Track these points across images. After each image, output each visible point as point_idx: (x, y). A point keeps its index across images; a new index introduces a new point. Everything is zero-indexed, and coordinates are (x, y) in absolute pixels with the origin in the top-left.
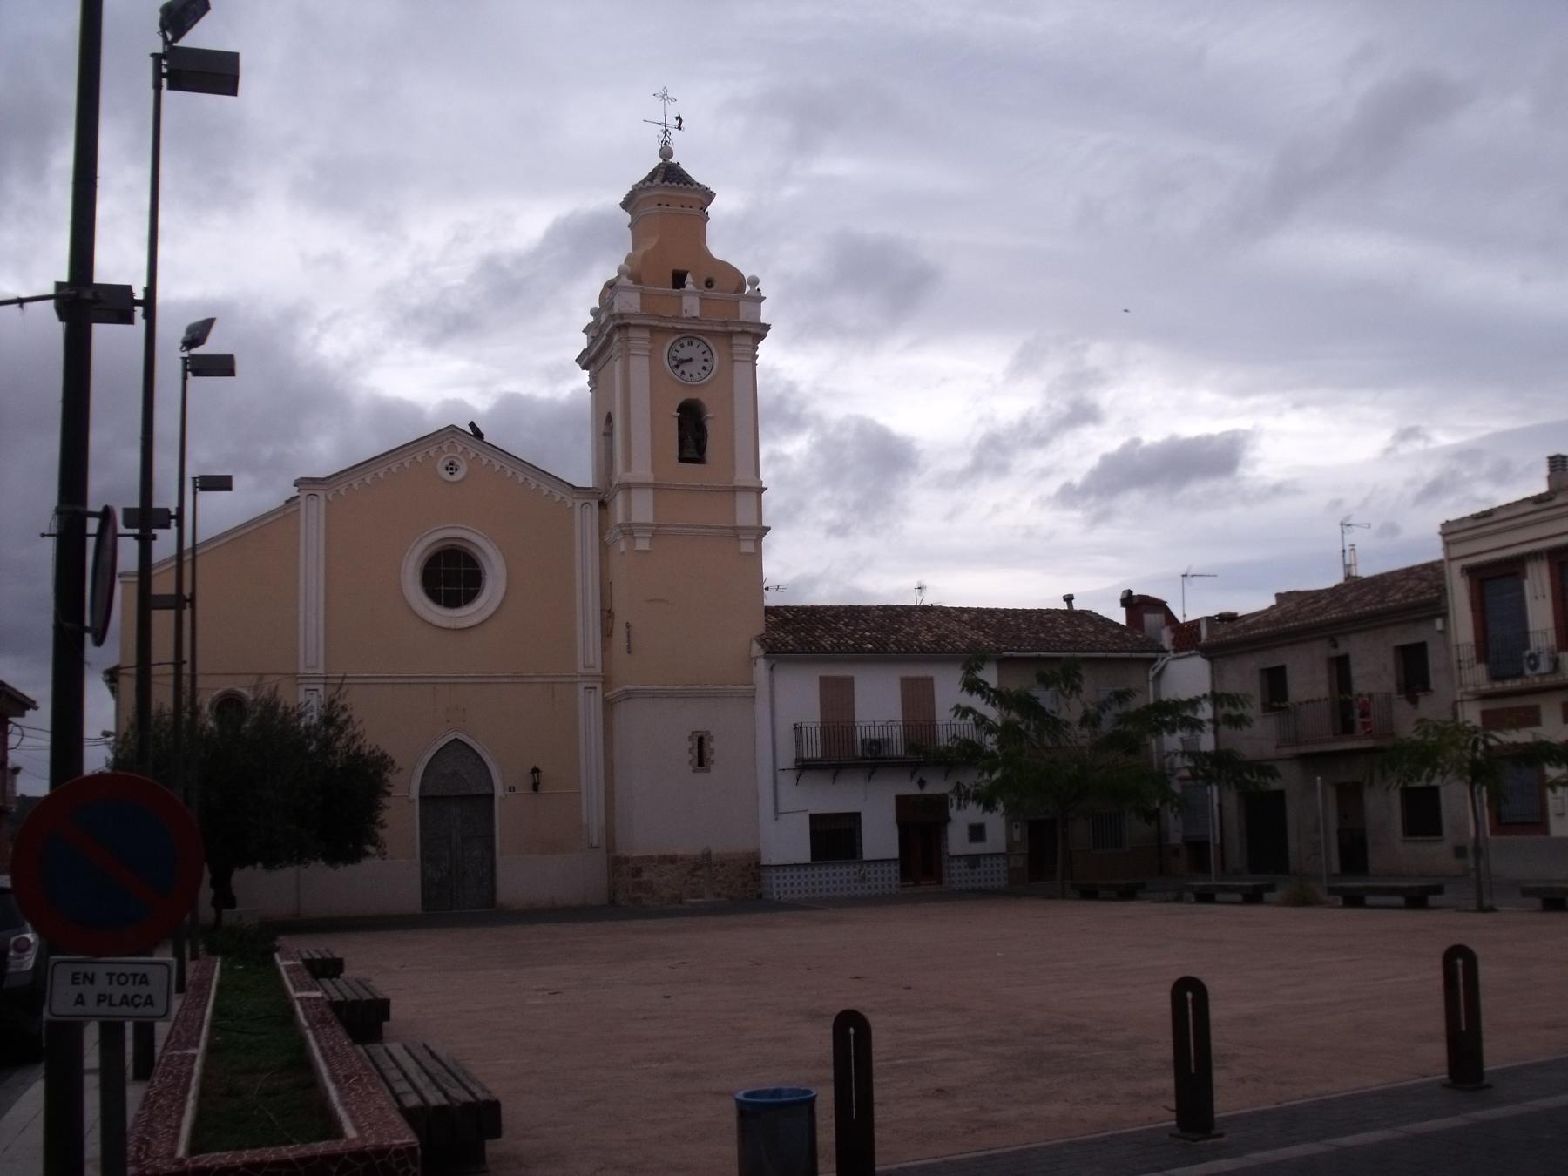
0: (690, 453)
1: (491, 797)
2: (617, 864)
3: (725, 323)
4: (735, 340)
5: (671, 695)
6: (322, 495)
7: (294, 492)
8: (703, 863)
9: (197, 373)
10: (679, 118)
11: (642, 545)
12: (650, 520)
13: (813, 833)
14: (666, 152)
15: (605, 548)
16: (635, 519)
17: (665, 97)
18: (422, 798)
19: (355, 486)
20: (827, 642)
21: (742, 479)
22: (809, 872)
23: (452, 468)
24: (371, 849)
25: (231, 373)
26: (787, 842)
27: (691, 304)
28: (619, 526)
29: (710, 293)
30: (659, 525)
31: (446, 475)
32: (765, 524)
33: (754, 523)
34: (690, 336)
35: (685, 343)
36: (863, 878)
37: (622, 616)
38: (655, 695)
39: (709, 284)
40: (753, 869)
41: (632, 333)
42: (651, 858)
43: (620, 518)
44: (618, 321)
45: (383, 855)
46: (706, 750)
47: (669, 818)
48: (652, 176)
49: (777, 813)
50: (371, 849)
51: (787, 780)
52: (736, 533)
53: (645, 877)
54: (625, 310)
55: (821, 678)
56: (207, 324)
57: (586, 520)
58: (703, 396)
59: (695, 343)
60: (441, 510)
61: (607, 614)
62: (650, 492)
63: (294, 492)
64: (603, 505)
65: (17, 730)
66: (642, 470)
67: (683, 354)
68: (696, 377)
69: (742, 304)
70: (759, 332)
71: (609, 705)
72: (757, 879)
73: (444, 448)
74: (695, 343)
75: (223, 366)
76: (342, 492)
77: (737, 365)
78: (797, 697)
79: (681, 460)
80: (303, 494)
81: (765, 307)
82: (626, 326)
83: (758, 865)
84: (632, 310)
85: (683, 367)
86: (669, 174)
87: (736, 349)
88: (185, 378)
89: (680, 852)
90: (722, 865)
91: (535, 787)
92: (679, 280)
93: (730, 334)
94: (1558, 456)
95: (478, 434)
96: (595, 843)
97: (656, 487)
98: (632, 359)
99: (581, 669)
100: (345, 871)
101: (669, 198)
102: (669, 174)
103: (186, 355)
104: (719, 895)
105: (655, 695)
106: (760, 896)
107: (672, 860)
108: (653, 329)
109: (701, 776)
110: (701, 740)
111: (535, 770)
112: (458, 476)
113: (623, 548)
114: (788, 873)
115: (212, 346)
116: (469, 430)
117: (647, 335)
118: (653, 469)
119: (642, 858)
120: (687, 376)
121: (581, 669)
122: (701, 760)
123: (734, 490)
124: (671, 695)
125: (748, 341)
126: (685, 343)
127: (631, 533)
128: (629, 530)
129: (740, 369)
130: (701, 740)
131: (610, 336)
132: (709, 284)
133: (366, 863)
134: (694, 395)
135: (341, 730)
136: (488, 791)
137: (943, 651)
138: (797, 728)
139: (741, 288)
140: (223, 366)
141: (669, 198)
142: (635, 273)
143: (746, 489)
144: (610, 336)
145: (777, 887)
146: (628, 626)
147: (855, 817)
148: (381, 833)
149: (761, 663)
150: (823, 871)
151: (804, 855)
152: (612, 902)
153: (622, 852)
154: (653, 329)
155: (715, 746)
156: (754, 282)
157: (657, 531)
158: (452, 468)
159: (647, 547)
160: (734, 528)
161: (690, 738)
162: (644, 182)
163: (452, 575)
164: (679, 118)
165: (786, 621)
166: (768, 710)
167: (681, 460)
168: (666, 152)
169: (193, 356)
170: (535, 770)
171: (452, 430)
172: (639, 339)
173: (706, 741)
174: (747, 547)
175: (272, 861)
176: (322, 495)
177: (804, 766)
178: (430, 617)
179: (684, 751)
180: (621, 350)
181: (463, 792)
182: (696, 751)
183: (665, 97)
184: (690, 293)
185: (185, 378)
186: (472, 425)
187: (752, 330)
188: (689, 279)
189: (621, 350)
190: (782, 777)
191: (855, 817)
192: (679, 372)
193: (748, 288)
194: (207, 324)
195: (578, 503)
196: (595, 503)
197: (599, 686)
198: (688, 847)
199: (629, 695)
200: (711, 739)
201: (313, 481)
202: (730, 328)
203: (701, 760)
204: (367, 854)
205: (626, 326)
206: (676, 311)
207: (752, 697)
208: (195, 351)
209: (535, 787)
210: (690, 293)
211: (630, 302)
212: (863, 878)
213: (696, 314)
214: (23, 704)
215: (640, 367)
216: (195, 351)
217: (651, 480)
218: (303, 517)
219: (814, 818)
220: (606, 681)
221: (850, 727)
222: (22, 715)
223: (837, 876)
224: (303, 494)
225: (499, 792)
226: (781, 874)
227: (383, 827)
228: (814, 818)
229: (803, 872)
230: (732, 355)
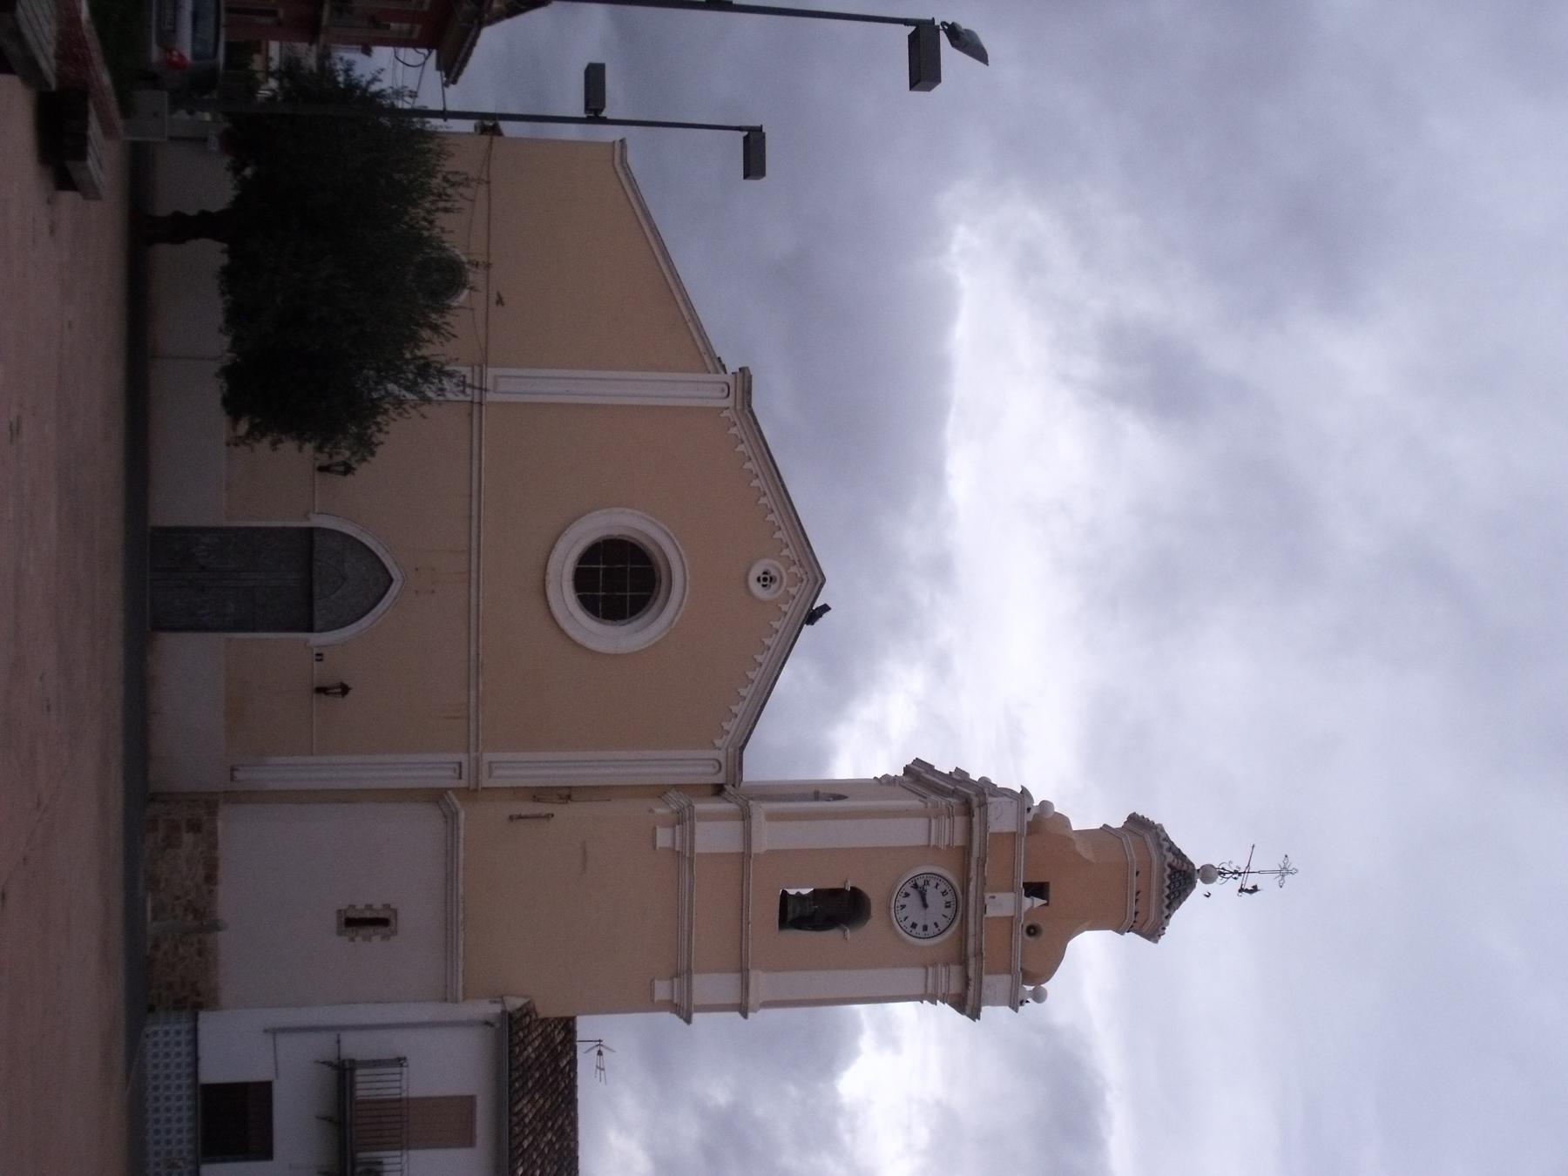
1: (310, 629)
2: (210, 803)
3: (979, 953)
4: (955, 969)
5: (450, 878)
6: (729, 402)
7: (732, 366)
8: (203, 920)
9: (913, 39)
10: (1255, 889)
11: (664, 838)
12: (698, 850)
13: (243, 1086)
14: (1209, 874)
15: (660, 792)
16: (701, 827)
17: (1284, 871)
18: (311, 530)
19: (741, 448)
20: (524, 1105)
21: (761, 981)
22: (185, 1081)
23: (766, 579)
24: (243, 426)
25: (914, 85)
26: (231, 1048)
27: (1004, 904)
28: (690, 805)
29: (1020, 935)
30: (691, 860)
31: (757, 571)
32: (696, 1017)
33: (697, 999)
34: (959, 905)
35: (949, 898)
36: (173, 1165)
37: (561, 811)
38: (450, 853)
39: (1033, 931)
41: (960, 821)
42: (214, 846)
43: (700, 807)
44: (975, 801)
45: (236, 442)
46: (371, 930)
47: (271, 876)
48: (1179, 854)
49: (274, 1032)
50: (243, 426)
51: (322, 1046)
52: (682, 973)
53: (188, 838)
54: (991, 809)
55: (470, 1100)
56: (979, 54)
57: (699, 766)
59: (949, 912)
60: (707, 564)
61: (566, 795)
62: (736, 847)
63: (732, 366)
64: (718, 790)
65: (421, 59)
66: (768, 837)
67: (933, 895)
68: (902, 915)
69: (1007, 978)
70: (967, 1004)
71: (436, 796)
72: (179, 1005)
73: (793, 569)
74: (949, 912)
75: (924, 72)
76: (733, 430)
77: (920, 972)
78: (445, 1061)
80: (729, 379)
81: (1004, 1011)
82: (969, 813)
83: (198, 1007)
84: (991, 818)
85: (914, 894)
86: (1180, 878)
87: (942, 971)
88: (906, 22)
89: (222, 891)
90: (200, 953)
91: (321, 690)
92: (1036, 889)
93: (963, 962)
95: (813, 616)
96: (239, 775)
97: (745, 856)
98: (922, 822)
99: (488, 757)
100: (212, 392)
101: (1145, 879)
102: (1180, 878)
103: (937, 23)
104: (156, 946)
105: (450, 853)
106: (151, 1009)
107: (211, 878)
108: (966, 851)
109: (332, 921)
110: (384, 922)
111: (345, 690)
112: (756, 588)
113: (659, 811)
114: (184, 1049)
115: (950, 57)
116: (818, 604)
117: (959, 841)
118: (771, 853)
119: (213, 833)
120: (902, 901)
121: (488, 757)
122: (354, 923)
123: (743, 971)
124: (450, 878)
125: (955, 987)
126: (949, 898)
127: (680, 821)
128: (683, 819)
129: (914, 977)
130: (384, 922)
131: (954, 793)
132: (1033, 931)
133: (221, 419)
134: (875, 910)
135: (411, 387)
136: (318, 623)
137: (513, 1161)
138: (400, 1061)
139: (1029, 977)
140: (924, 72)
141: (1145, 879)
142: (1041, 824)
143: (745, 987)
144: (954, 793)
145: (164, 1031)
146: (549, 816)
147: (266, 1153)
148: (266, 442)
149: (497, 1009)
150: (186, 1103)
151: (211, 1073)
152: (153, 798)
153: (224, 811)
154: (966, 851)
155: (373, 945)
156: (1039, 997)
157: (682, 857)
158: (766, 579)
159: (659, 844)
160: (689, 970)
161: (387, 907)
162: (1167, 839)
163: (619, 579)
164: (1255, 889)
165: (556, 1057)
168: (1209, 874)
169: (938, 30)
170: (345, 690)
171: (819, 581)
172: (950, 832)
173: (382, 930)
174: (662, 991)
175: (230, 277)
176: (729, 402)
177: (343, 1072)
178: (561, 546)
179: (369, 898)
180: (936, 805)
181: (317, 590)
182: (368, 915)
183: (1284, 871)
184: (1019, 905)
185: (906, 22)
186: (825, 608)
187: (971, 993)
188: (1038, 902)
189: (936, 805)
190: (326, 1040)
191: (266, 1153)
192: (908, 889)
193: (1029, 988)
194: (979, 54)
195: (720, 755)
196: (720, 779)
197: (463, 783)
198: (228, 900)
199: (451, 818)
200: (386, 937)
201: (747, 392)
202: (972, 961)
203: (354, 923)
204: (236, 420)
205: (969, 813)
206: (984, 893)
207: (447, 997)
208: (943, 38)
209: (321, 690)
210: (1019, 905)
211: (1002, 820)
212: (173, 1165)
213: (990, 913)
214: (452, 68)
215: (912, 833)
216: (943, 38)
217: (755, 850)
218: (691, 376)
219: (265, 1089)
220: (471, 793)
221: (403, 1143)
222: (439, 67)
223: (176, 1124)
224: (729, 379)
225: (317, 639)
226: (184, 1038)
227: (274, 445)
228: (265, 1089)
230: (934, 965)
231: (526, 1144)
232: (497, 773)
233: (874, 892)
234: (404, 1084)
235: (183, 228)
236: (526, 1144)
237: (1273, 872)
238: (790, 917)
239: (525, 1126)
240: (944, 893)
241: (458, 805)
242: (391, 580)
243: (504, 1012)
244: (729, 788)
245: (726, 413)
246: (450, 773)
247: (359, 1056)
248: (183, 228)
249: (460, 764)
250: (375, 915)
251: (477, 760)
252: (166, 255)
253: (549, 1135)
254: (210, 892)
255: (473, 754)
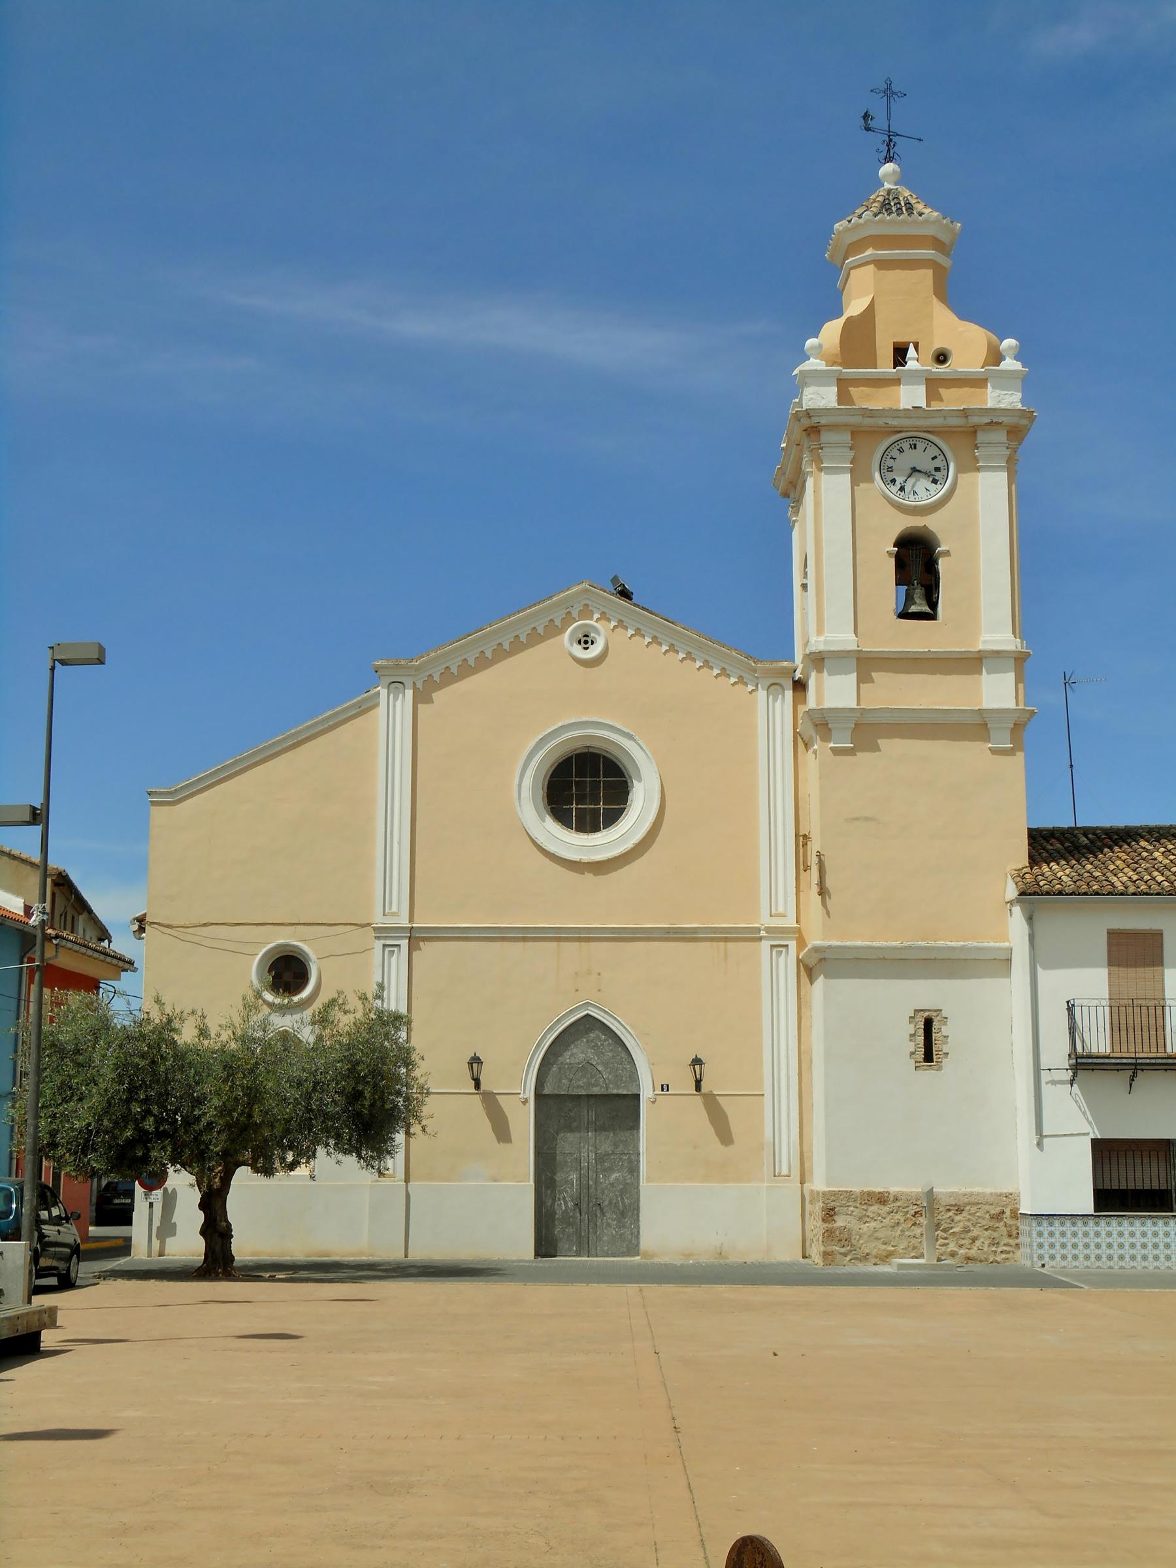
0: (920, 606)
1: (637, 1097)
18: (539, 1096)
22: (1091, 1227)
31: (578, 651)
40: (1004, 1216)
53: (840, 1222)
55: (1111, 934)
58: (933, 523)
61: (802, 840)
74: (921, 445)
79: (931, 617)
90: (960, 1211)
93: (974, 431)
94: (749, 1537)
107: (882, 1199)
109: (928, 1075)
110: (928, 1023)
111: (697, 1062)
112: (594, 651)
114: (1057, 1227)
130: (928, 1023)
132: (941, 357)
149: (1017, 910)
151: (1087, 1204)
154: (856, 432)
155: (948, 1034)
166: (152, 1284)
167: (904, 615)
170: (697, 1062)
172: (836, 442)
179: (907, 1041)
181: (596, 1090)
182: (921, 1039)
188: (911, 353)
225: (646, 1093)
229: (1080, 1227)
231: (1160, 879)
232: (781, 910)
233: (901, 524)
234: (1095, 1003)
235: (216, 1230)
236: (1160, 879)
237: (889, 103)
238: (926, 609)
239: (1141, 879)
240: (901, 451)
241: (809, 946)
242: (588, 1015)
243: (1018, 901)
244: (798, 675)
245: (419, 685)
246: (782, 959)
247: (1067, 1050)
248: (216, 1230)
249: (772, 946)
250: (921, 1031)
251: (768, 930)
252: (245, 1246)
253: (1156, 854)
254: (896, 1199)
255: (763, 933)
